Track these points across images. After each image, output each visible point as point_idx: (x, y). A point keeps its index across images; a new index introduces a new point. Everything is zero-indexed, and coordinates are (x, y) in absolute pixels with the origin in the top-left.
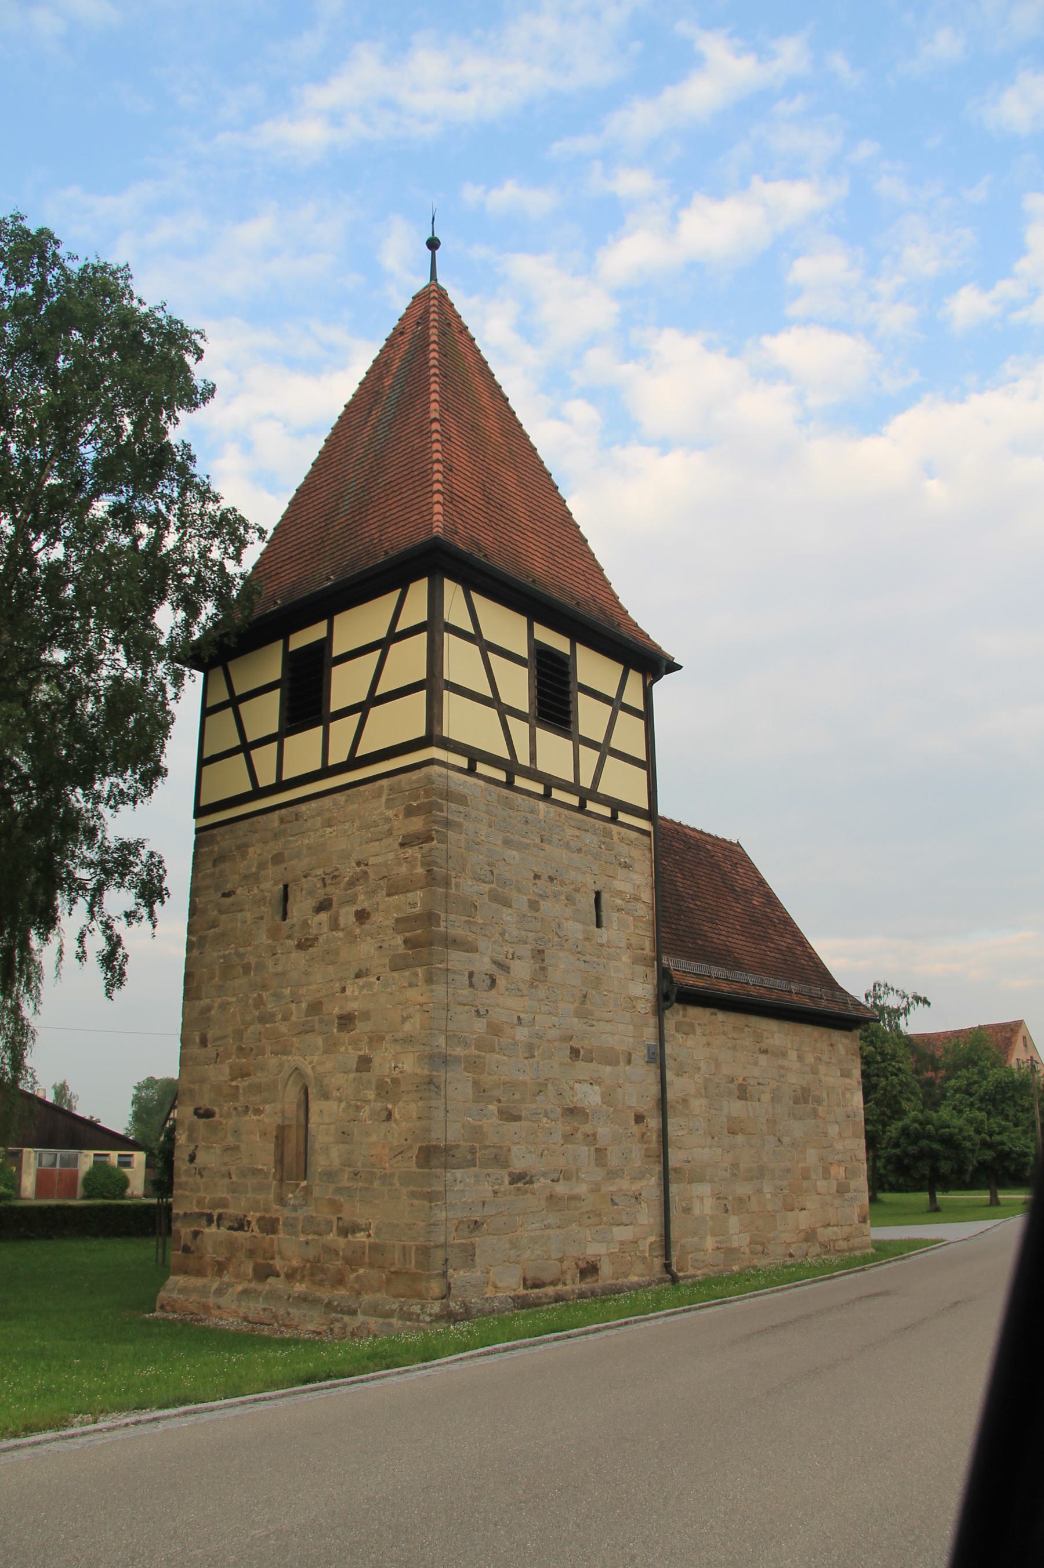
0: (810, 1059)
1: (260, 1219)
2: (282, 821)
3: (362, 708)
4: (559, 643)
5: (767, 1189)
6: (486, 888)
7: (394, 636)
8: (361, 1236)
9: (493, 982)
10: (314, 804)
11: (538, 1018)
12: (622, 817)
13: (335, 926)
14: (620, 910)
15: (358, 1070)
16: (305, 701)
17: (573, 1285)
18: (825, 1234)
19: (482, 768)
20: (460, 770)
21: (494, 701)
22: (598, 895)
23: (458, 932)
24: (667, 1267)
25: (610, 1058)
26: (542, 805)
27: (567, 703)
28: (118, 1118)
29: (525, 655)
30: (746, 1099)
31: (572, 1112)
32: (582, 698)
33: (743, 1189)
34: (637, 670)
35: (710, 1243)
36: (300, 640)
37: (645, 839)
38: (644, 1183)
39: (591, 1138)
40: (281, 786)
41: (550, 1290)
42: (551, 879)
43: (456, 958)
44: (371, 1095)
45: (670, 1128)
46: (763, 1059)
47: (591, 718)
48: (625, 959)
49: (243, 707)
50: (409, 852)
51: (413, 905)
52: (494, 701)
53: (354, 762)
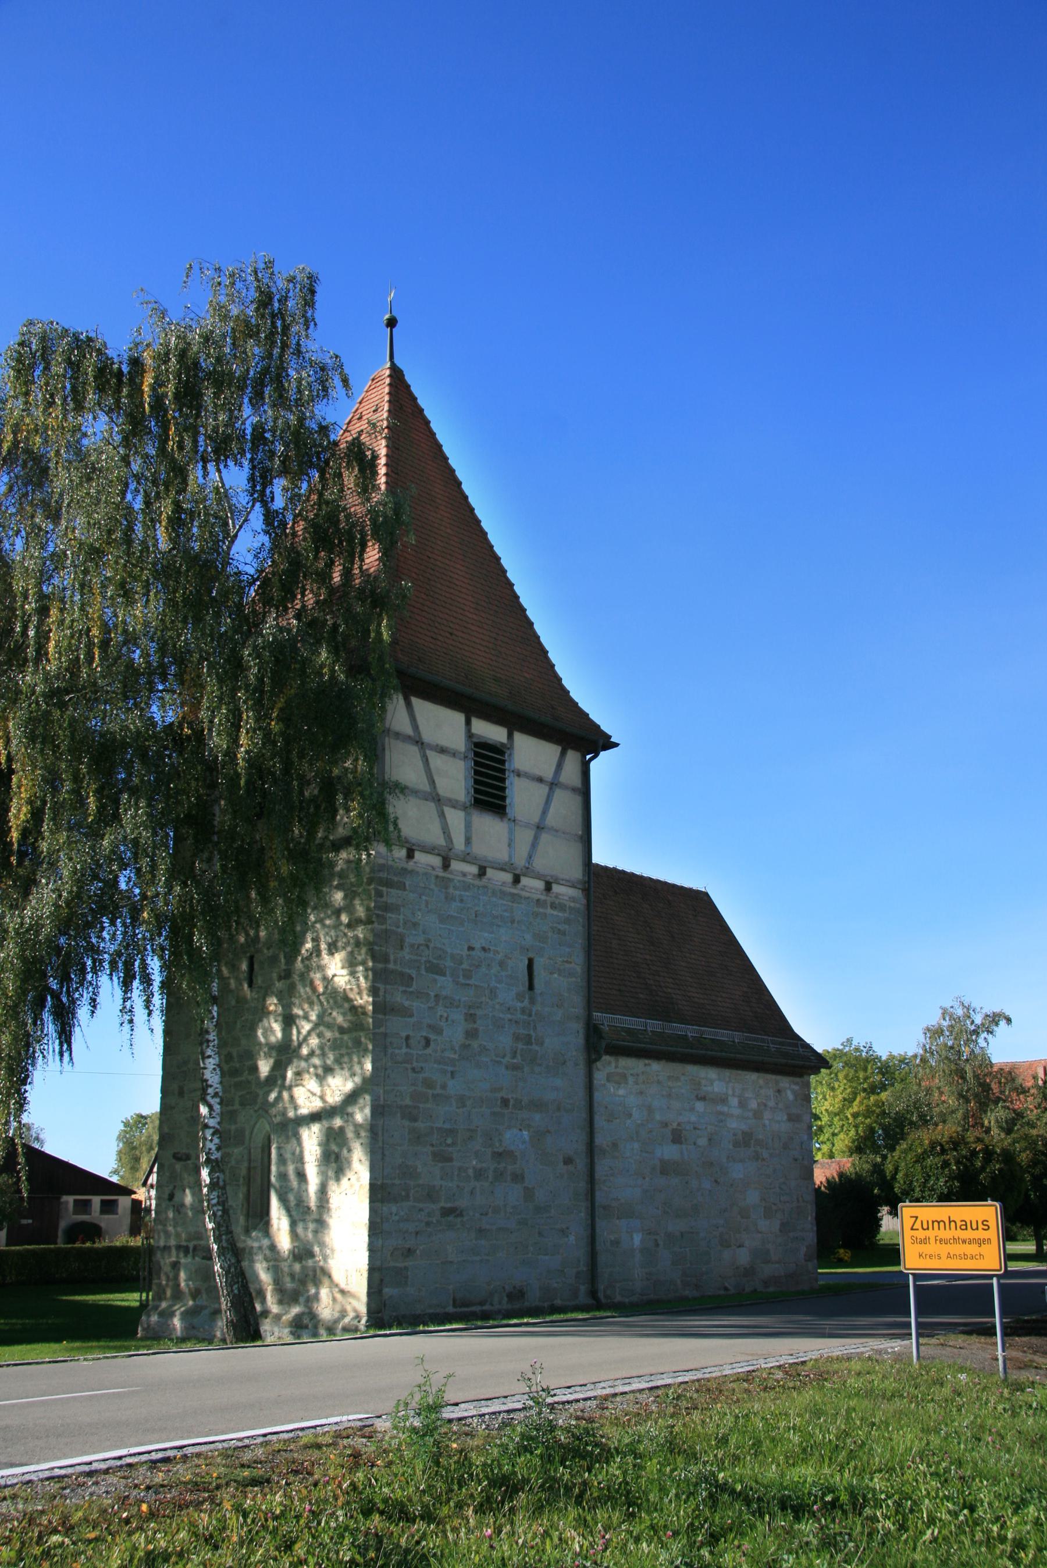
4: (493, 733)
30: (681, 1143)
34: (573, 748)
45: (598, 1168)
46: (700, 1106)
47: (523, 797)
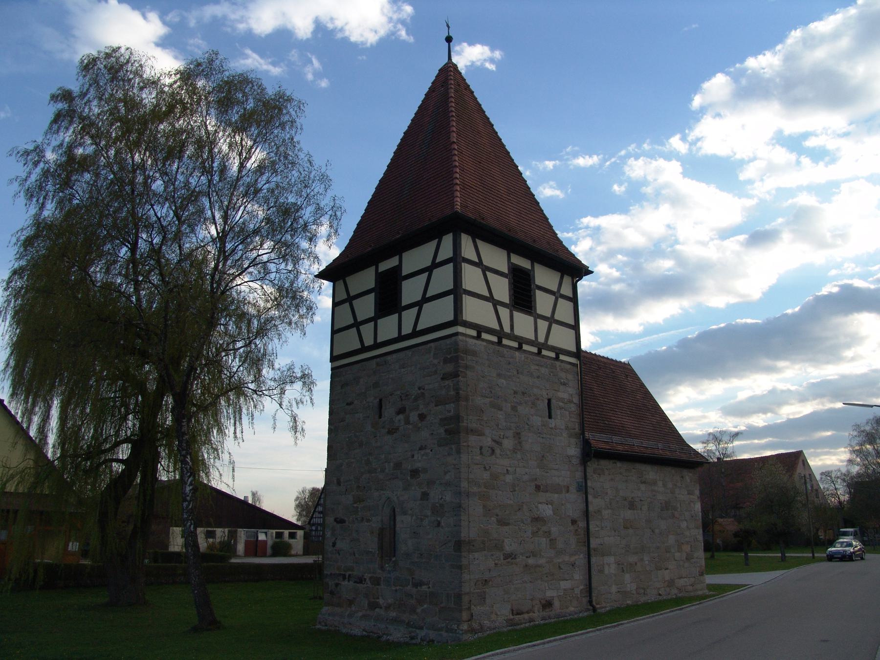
0: (670, 485)
1: (371, 578)
2: (378, 364)
3: (419, 304)
5: (646, 558)
6: (488, 400)
7: (435, 265)
8: (424, 588)
9: (493, 451)
10: (394, 356)
11: (518, 469)
12: (562, 357)
13: (407, 422)
14: (561, 408)
15: (421, 499)
16: (388, 299)
17: (538, 615)
18: (681, 583)
19: (484, 336)
20: (473, 337)
21: (490, 299)
22: (549, 401)
23: (474, 425)
24: (590, 602)
25: (557, 489)
26: (517, 353)
27: (530, 297)
28: (289, 513)
29: (506, 271)
31: (537, 520)
32: (538, 292)
33: (632, 559)
35: (614, 589)
36: (384, 266)
37: (575, 369)
38: (577, 557)
39: (548, 533)
40: (377, 345)
41: (526, 616)
42: (524, 393)
43: (473, 439)
44: (429, 513)
45: (591, 527)
46: (643, 487)
47: (543, 303)
48: (565, 435)
49: (355, 303)
50: (447, 382)
51: (449, 411)
52: (490, 299)
53: (415, 334)
